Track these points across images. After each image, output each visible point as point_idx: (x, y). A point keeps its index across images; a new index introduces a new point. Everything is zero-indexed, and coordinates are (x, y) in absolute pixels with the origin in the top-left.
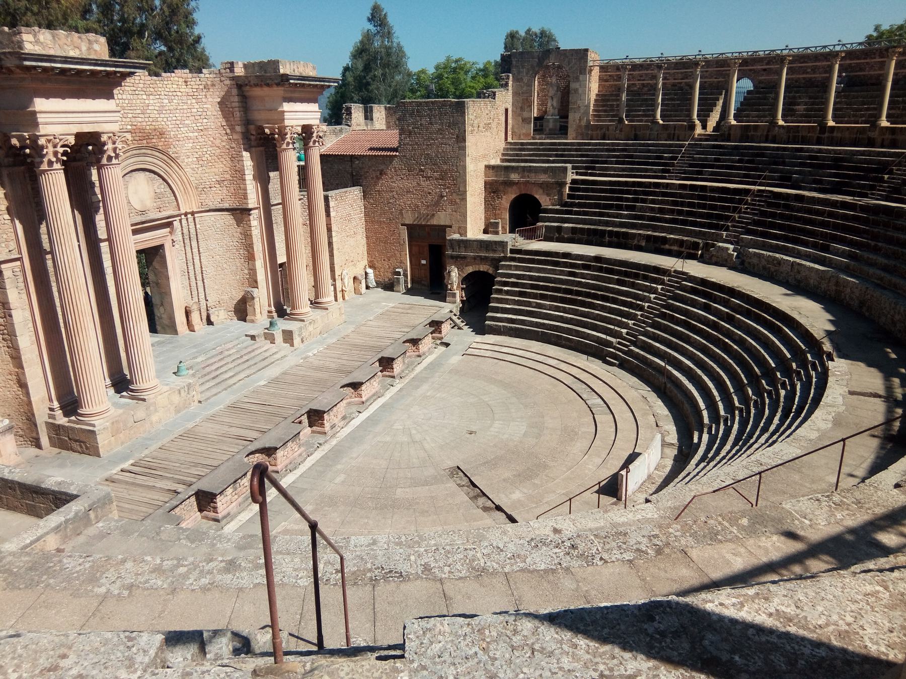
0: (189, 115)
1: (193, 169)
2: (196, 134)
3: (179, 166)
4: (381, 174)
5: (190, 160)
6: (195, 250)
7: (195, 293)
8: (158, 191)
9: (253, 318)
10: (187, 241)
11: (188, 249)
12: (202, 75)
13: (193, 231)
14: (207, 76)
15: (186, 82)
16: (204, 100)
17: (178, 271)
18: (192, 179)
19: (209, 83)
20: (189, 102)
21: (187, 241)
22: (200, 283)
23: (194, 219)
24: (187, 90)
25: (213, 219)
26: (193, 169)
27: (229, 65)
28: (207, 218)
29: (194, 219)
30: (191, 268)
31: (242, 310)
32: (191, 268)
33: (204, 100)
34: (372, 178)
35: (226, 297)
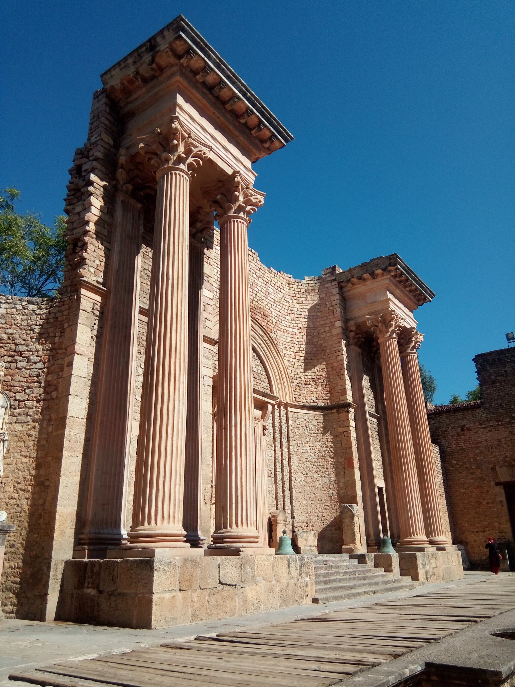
0: (289, 312)
1: (289, 361)
2: (296, 330)
3: (278, 352)
4: (463, 430)
5: (288, 352)
6: (285, 449)
7: (281, 503)
8: (255, 370)
9: (351, 546)
10: (278, 436)
11: (278, 445)
12: (304, 281)
13: (284, 426)
14: (309, 282)
15: (289, 284)
16: (304, 302)
17: (266, 471)
18: (289, 371)
19: (310, 288)
20: (291, 301)
21: (278, 436)
22: (287, 492)
23: (287, 414)
24: (289, 291)
25: (306, 418)
26: (289, 361)
27: (331, 270)
28: (300, 416)
29: (287, 414)
30: (279, 470)
31: (333, 539)
32: (279, 470)
33: (304, 302)
34: (453, 436)
35: (315, 518)
